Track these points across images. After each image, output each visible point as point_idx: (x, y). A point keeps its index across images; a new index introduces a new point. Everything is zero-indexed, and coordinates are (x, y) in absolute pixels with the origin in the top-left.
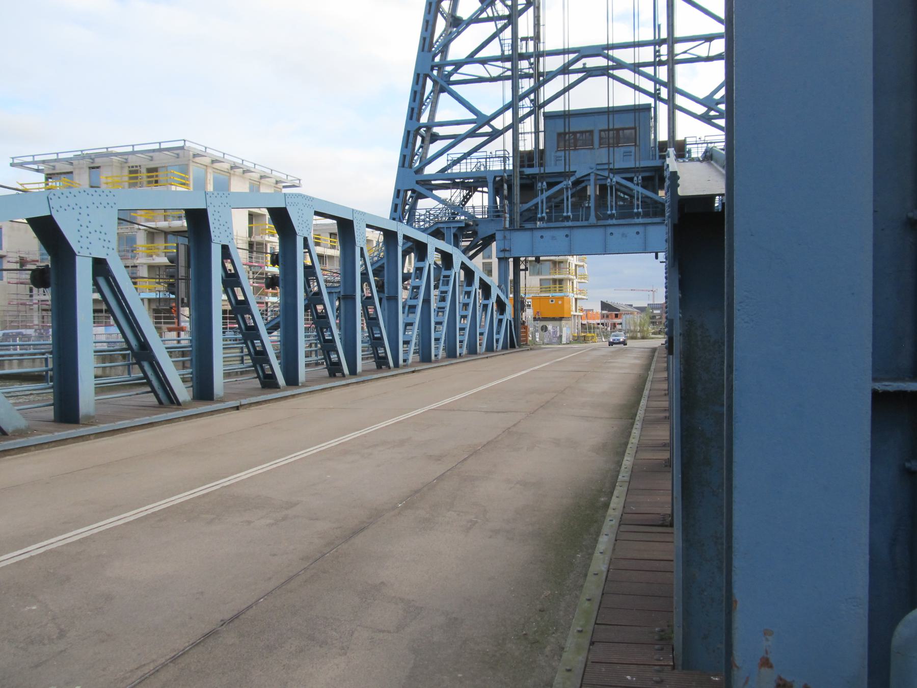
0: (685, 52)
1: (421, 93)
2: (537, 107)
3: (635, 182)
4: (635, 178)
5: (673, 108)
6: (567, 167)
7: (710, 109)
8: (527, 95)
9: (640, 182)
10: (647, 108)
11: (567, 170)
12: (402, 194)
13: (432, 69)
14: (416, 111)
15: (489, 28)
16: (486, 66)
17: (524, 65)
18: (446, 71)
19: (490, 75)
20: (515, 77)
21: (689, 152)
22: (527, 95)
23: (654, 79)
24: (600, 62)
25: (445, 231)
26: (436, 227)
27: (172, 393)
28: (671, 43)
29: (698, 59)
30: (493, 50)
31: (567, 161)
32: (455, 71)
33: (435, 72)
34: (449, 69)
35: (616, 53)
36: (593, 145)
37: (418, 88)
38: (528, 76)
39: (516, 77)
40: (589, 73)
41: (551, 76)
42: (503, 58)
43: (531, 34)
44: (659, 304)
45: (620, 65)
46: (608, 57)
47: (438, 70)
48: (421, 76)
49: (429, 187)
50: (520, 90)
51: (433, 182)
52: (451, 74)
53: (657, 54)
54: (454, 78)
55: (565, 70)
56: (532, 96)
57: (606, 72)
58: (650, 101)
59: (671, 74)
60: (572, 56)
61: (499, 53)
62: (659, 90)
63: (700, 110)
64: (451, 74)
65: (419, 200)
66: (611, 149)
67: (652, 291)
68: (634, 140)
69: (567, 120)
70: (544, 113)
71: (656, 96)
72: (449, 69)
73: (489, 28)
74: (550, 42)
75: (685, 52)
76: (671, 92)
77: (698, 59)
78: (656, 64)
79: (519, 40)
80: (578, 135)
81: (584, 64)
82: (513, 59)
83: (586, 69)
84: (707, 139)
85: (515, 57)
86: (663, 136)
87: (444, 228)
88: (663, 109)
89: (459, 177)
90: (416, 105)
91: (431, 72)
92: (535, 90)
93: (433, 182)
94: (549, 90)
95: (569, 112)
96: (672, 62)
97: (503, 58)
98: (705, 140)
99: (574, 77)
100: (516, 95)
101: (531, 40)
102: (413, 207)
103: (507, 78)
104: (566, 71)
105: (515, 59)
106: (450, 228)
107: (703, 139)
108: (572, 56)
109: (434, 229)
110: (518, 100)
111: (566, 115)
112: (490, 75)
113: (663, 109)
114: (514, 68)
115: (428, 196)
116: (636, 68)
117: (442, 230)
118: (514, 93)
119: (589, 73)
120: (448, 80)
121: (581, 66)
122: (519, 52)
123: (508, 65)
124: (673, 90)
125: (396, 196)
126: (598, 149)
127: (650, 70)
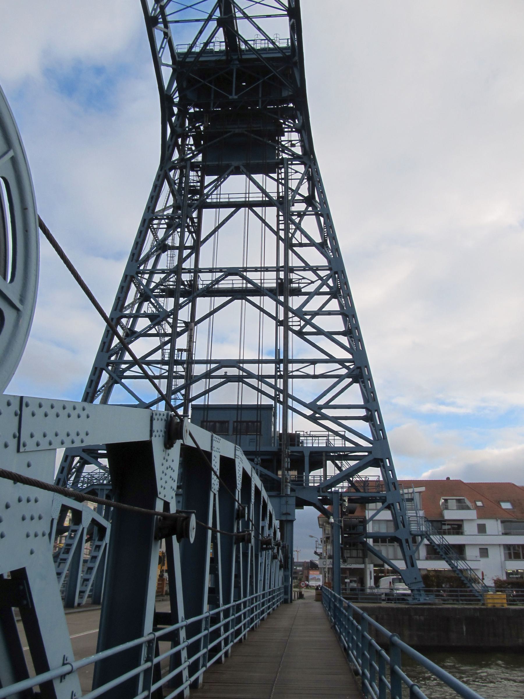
0: (297, 370)
1: (96, 382)
2: (187, 399)
3: (256, 462)
4: (256, 460)
5: (286, 407)
6: (258, 447)
7: (315, 412)
8: (178, 390)
9: (259, 462)
10: (269, 408)
11: (258, 450)
12: (69, 459)
13: (108, 365)
14: (90, 395)
15: (156, 342)
16: (150, 366)
17: (179, 369)
18: (121, 368)
19: (153, 373)
20: (171, 377)
21: (302, 443)
22: (178, 390)
23: (274, 387)
24: (233, 371)
25: (99, 492)
26: (92, 488)
27: (253, 582)
28: (286, 362)
29: (308, 376)
30: (157, 356)
31: (258, 442)
32: (128, 369)
33: (110, 368)
34: (124, 366)
35: (246, 366)
36: (228, 432)
37: (95, 378)
38: (181, 377)
39: (171, 377)
40: (229, 379)
41: (198, 378)
42: (163, 362)
43: (185, 347)
44: (301, 562)
45: (250, 375)
46: (240, 368)
47: (112, 366)
48: (98, 369)
49: (95, 455)
50: (173, 387)
51: (99, 452)
52: (125, 370)
53: (277, 369)
54: (127, 374)
55: (207, 375)
56: (183, 392)
57: (241, 380)
58: (272, 402)
59: (286, 384)
60: (213, 366)
61: (160, 358)
62: (279, 395)
63: (309, 412)
64: (125, 370)
65: (86, 465)
66: (238, 436)
67: (297, 551)
68: (258, 431)
69: (259, 412)
70: (192, 405)
71: (275, 399)
72: (124, 366)
73: (156, 342)
74: (199, 354)
75: (297, 370)
76: (285, 397)
77: (308, 376)
78: (277, 377)
79: (176, 351)
80: (250, 424)
81: (226, 373)
82: (170, 363)
83: (227, 376)
84: (312, 433)
85: (172, 362)
86: (279, 429)
87: (98, 489)
88: (280, 408)
89: (342, 450)
90: (91, 391)
91: (106, 367)
92: (187, 387)
93: (99, 452)
94: (196, 389)
95: (258, 407)
96: (286, 376)
97: (163, 362)
98: (310, 434)
99: (214, 382)
100: (169, 390)
101: (184, 352)
102: (80, 470)
103: (164, 377)
104: (208, 377)
105: (172, 364)
106: (103, 489)
107: (309, 433)
108: (213, 366)
109: (90, 489)
110: (170, 394)
111: (207, 408)
112: (153, 373)
113: (280, 408)
114: (170, 371)
115: (91, 462)
116: (261, 378)
117: (96, 491)
118: (168, 389)
119: (229, 379)
120: (121, 374)
121: (224, 374)
122: (175, 358)
123: (166, 367)
124: (287, 396)
125: (64, 460)
126: (231, 435)
127: (272, 381)
